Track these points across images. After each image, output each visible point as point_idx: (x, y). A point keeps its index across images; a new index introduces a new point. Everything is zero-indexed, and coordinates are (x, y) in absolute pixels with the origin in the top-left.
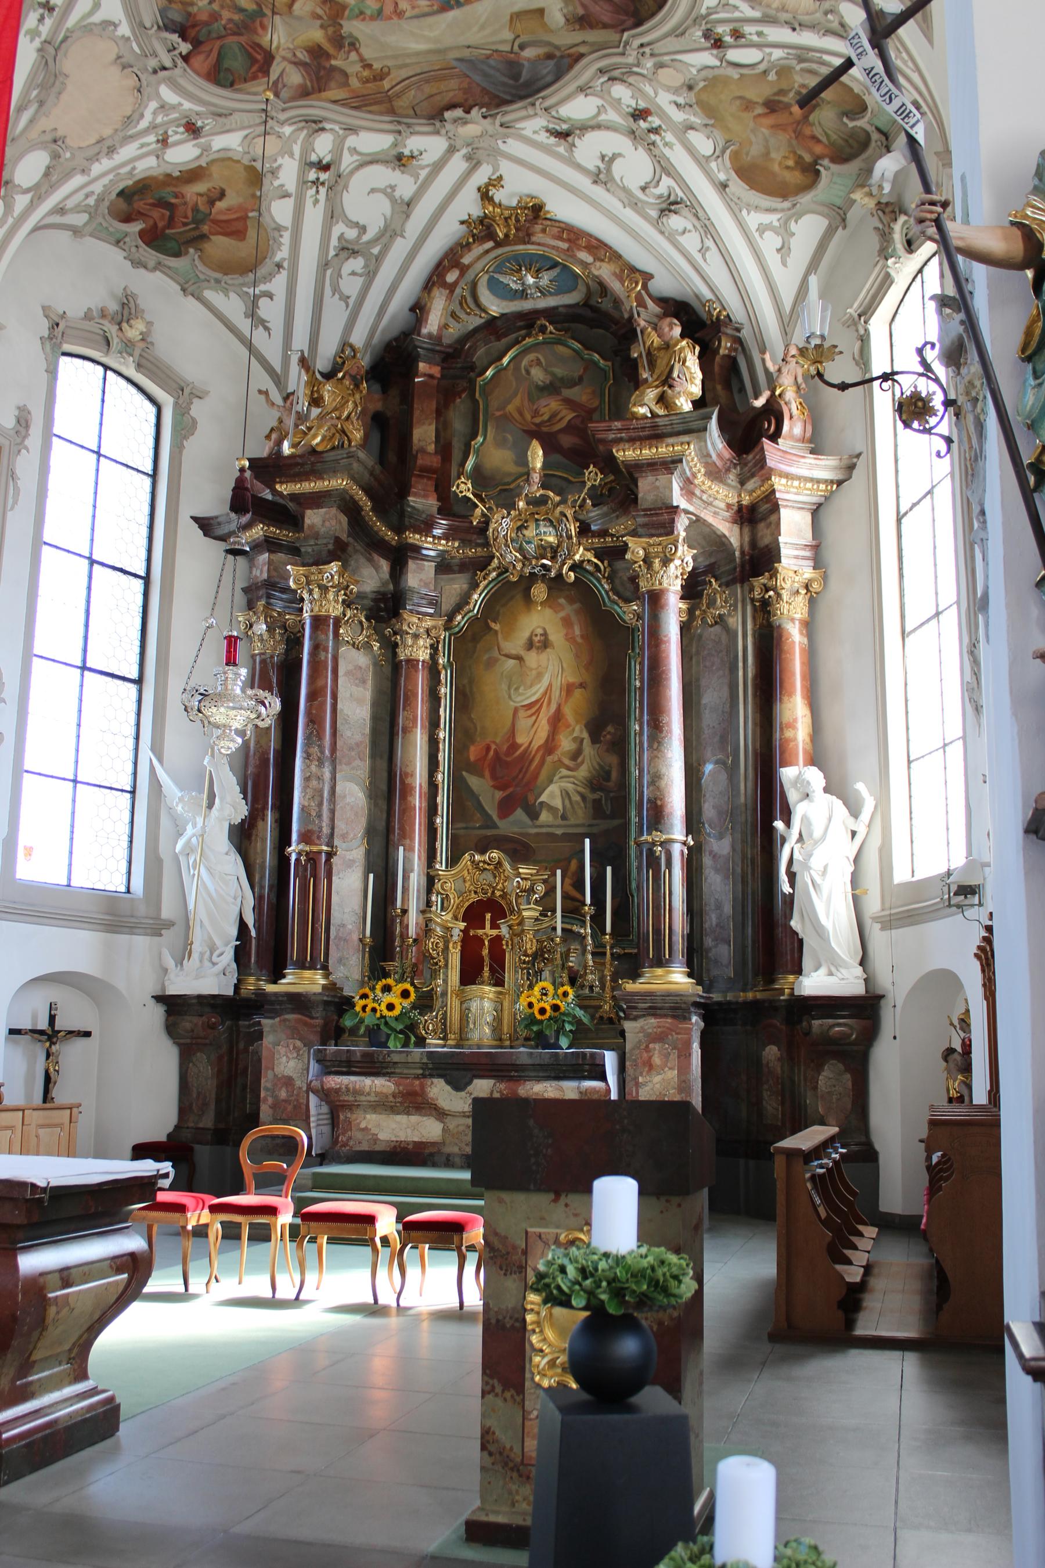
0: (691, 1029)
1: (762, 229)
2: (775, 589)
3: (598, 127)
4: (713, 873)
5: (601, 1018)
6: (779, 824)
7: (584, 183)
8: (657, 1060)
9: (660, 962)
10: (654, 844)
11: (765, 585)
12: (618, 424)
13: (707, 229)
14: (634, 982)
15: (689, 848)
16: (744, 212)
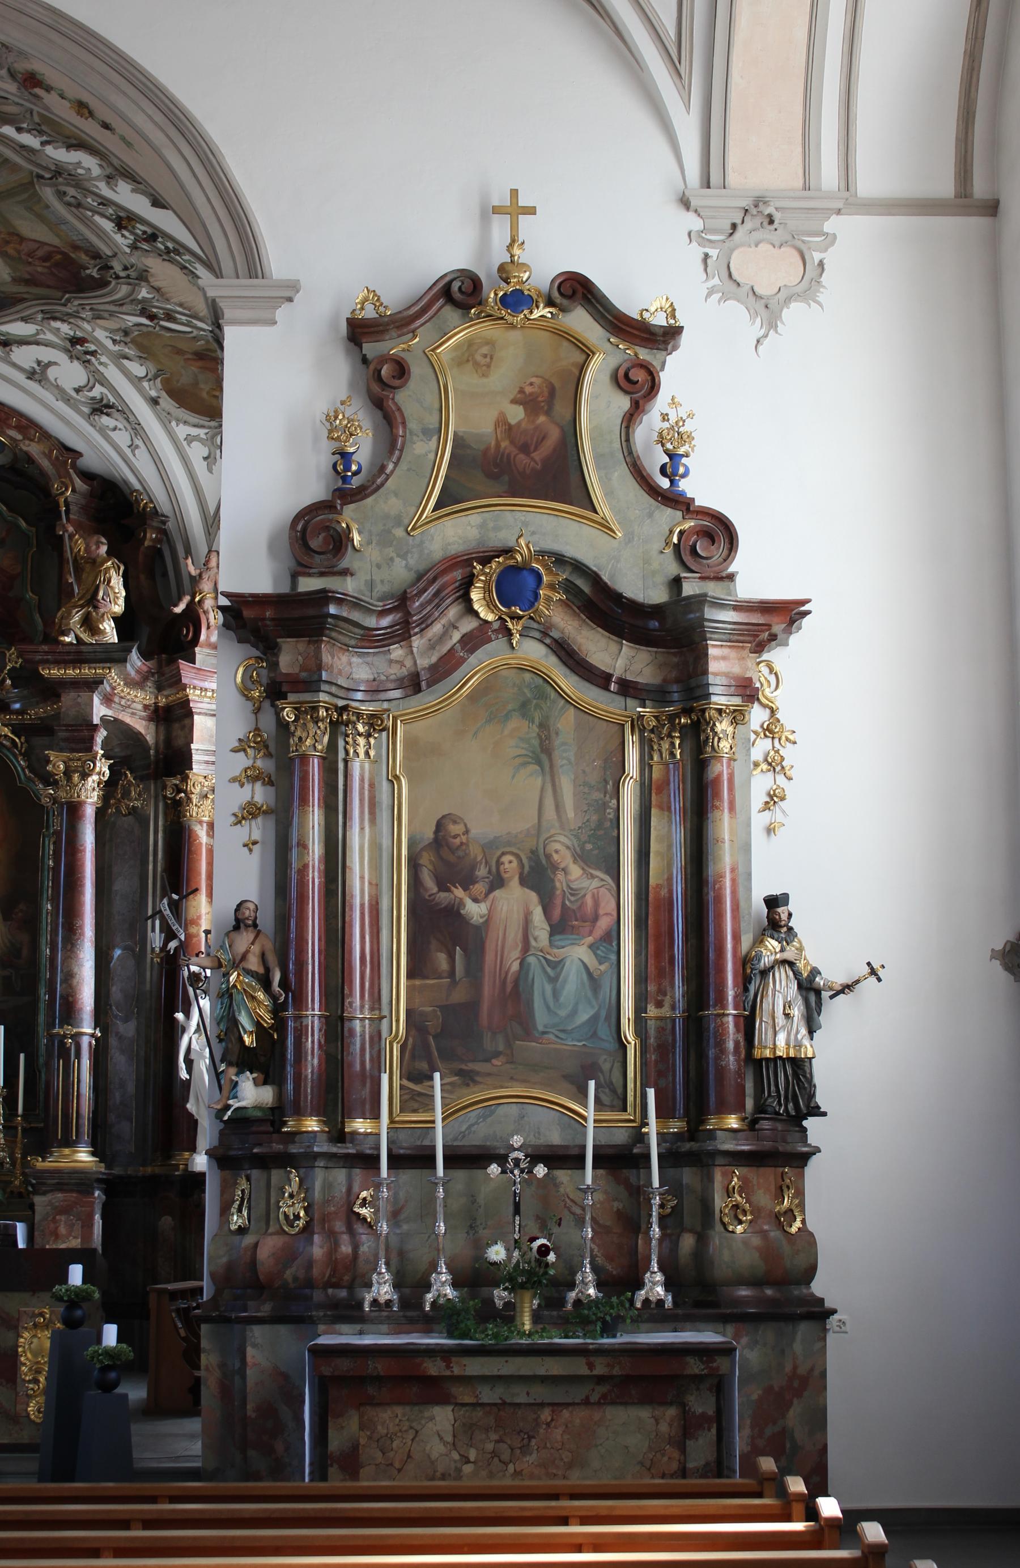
0: (93, 1203)
1: (190, 439)
2: (185, 792)
3: (38, 343)
4: (117, 1054)
5: (12, 1192)
6: (180, 1016)
7: (20, 378)
8: (63, 1230)
9: (69, 1142)
10: (65, 1036)
11: (176, 785)
12: (45, 648)
13: (137, 429)
14: (43, 1161)
15: (97, 1040)
16: (174, 424)
